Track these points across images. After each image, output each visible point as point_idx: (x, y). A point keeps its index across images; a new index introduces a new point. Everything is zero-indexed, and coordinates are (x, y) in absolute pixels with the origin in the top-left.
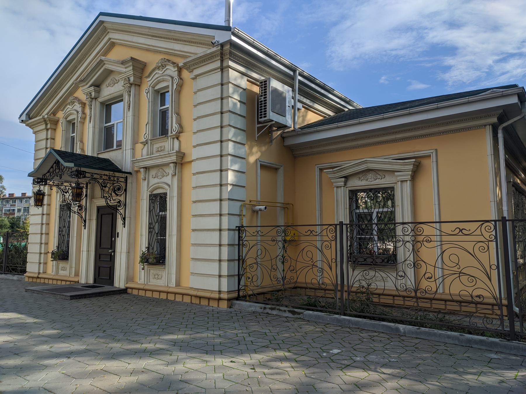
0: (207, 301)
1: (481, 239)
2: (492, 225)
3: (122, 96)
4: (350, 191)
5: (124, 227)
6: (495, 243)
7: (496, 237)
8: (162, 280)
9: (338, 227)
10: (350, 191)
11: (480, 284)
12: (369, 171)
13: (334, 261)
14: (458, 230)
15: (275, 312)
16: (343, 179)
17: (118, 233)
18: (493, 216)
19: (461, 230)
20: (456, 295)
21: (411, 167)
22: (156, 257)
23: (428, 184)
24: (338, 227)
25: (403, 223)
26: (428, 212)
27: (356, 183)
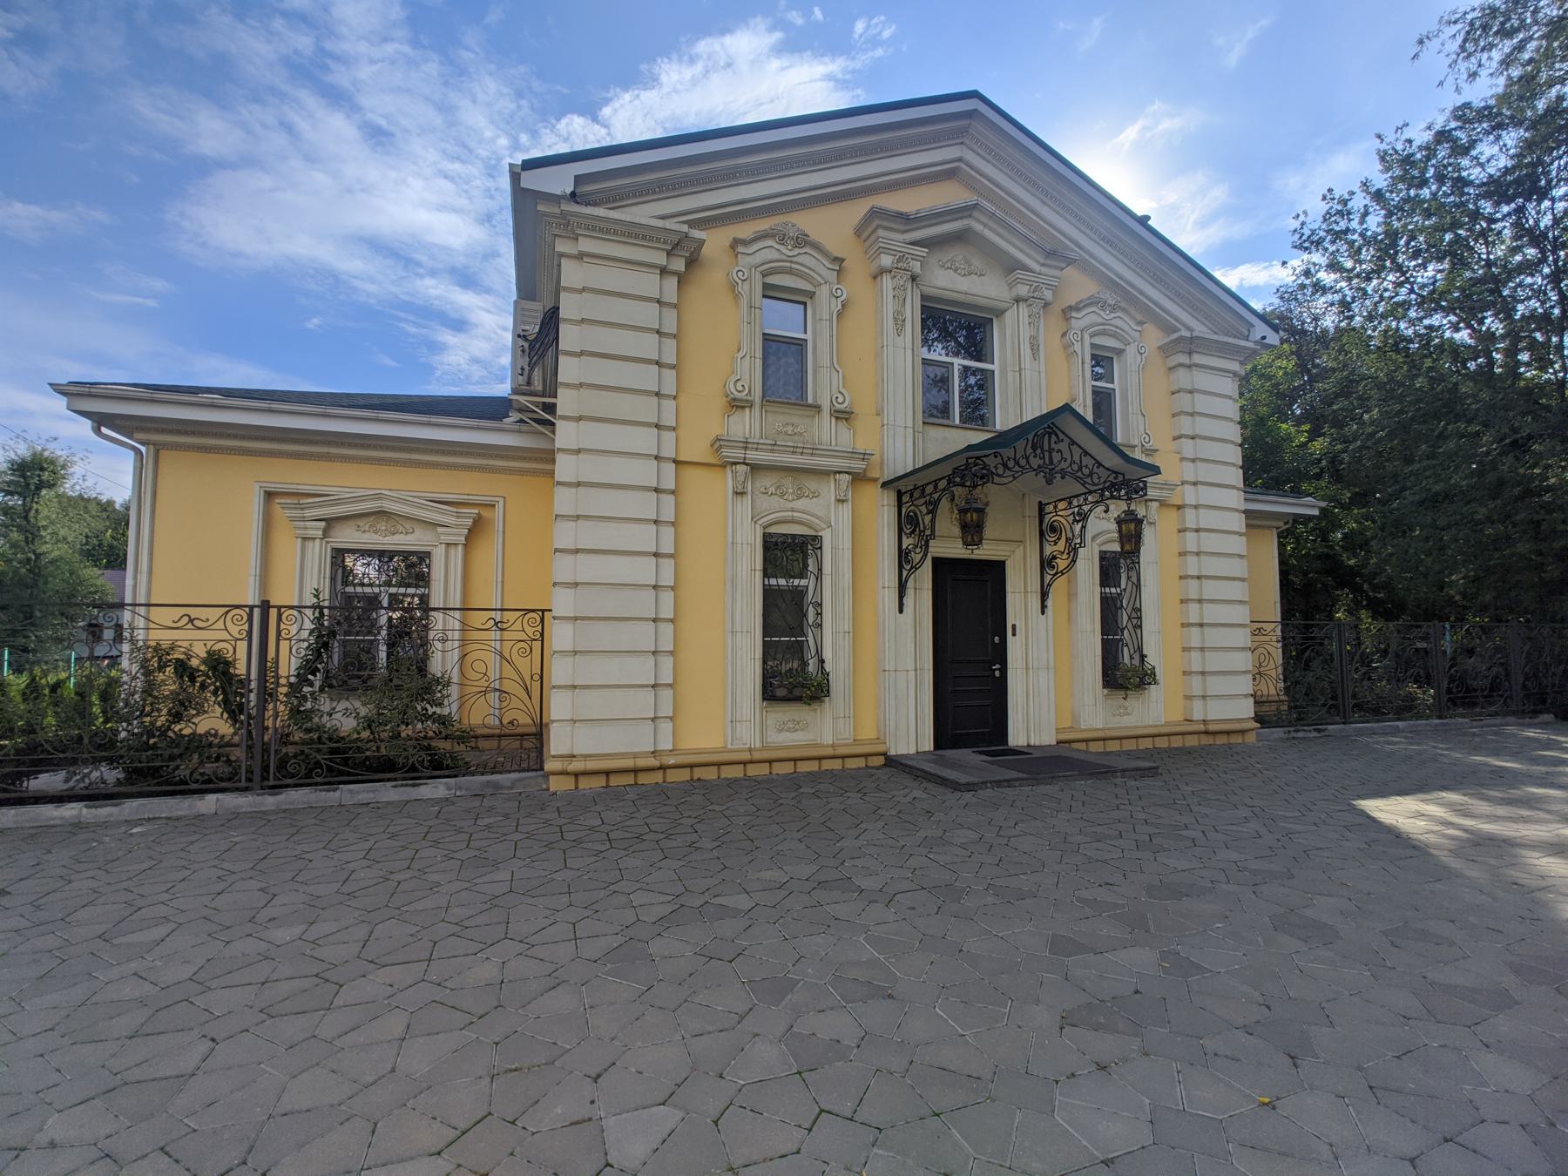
0: (573, 779)
1: (522, 636)
2: (244, 613)
3: (770, 341)
4: (333, 549)
5: (901, 611)
6: (245, 643)
7: (250, 633)
8: (1154, 711)
9: (257, 612)
10: (333, 549)
11: (515, 703)
12: (381, 514)
13: (536, 677)
14: (186, 619)
15: (1301, 735)
16: (323, 524)
17: (1014, 627)
18: (251, 598)
19: (191, 621)
20: (478, 726)
21: (469, 522)
22: (1123, 673)
23: (488, 555)
24: (257, 612)
25: (135, 605)
26: (488, 595)
27: (348, 536)
